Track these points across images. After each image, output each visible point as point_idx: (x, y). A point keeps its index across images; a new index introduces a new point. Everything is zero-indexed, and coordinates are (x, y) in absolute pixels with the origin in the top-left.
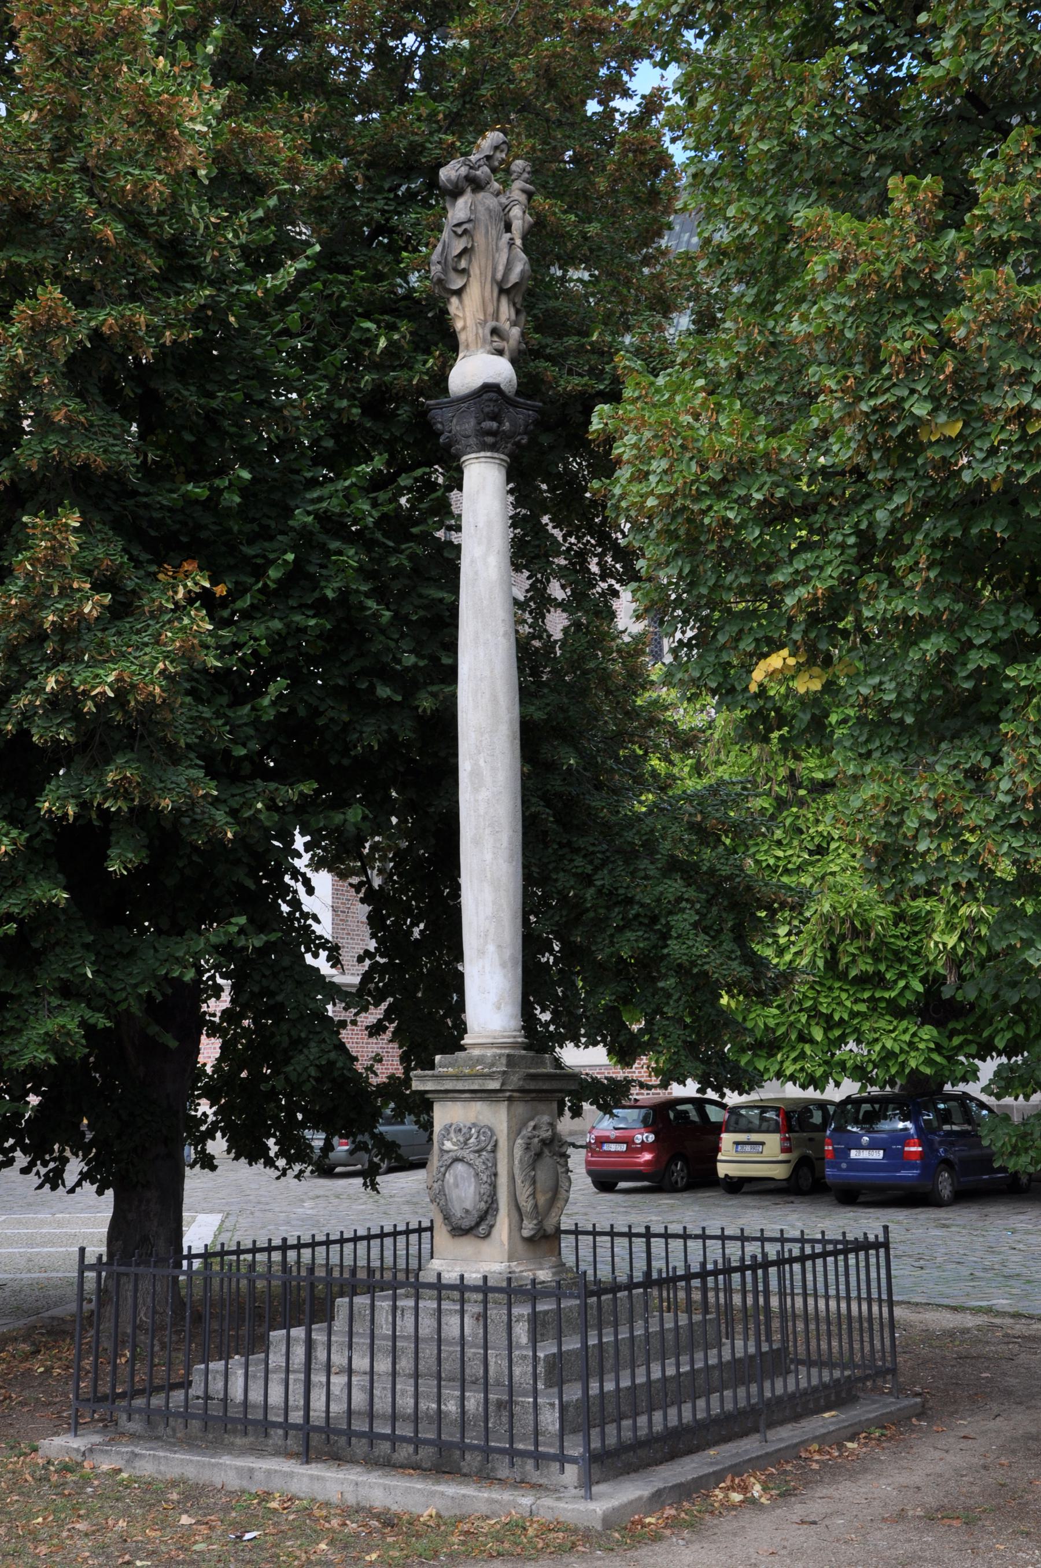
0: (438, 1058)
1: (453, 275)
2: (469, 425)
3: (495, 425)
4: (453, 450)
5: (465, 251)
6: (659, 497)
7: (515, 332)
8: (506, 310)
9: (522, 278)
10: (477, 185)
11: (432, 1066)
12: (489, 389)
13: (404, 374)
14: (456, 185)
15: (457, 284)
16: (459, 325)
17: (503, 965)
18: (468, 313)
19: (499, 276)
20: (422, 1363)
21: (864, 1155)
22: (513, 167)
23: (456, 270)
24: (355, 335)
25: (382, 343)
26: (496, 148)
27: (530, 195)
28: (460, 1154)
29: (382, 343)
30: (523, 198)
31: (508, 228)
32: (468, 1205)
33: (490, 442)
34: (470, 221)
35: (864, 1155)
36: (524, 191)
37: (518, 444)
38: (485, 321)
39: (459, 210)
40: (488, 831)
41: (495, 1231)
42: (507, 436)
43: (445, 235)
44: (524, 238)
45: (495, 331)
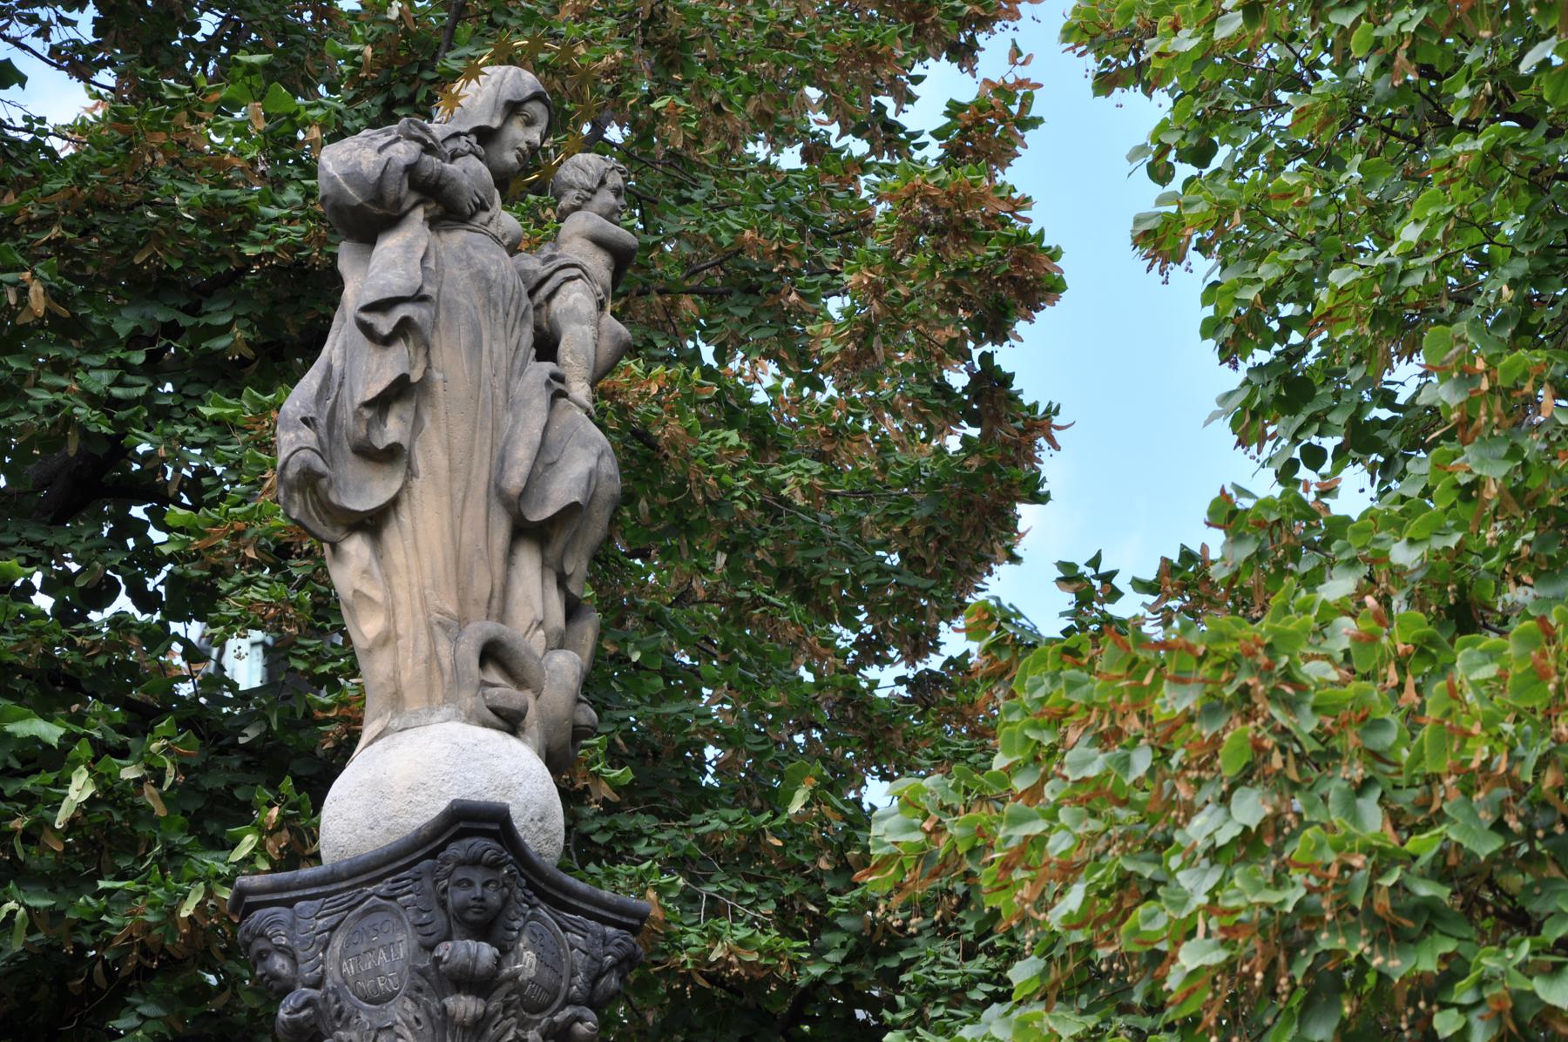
3: (486, 952)
5: (400, 391)
7: (564, 669)
8: (533, 598)
10: (448, 209)
12: (475, 824)
14: (377, 190)
16: (366, 628)
18: (398, 592)
19: (515, 480)
22: (567, 173)
25: (80, 788)
26: (513, 108)
29: (80, 788)
30: (599, 264)
31: (546, 346)
34: (419, 298)
36: (600, 242)
45: (492, 653)
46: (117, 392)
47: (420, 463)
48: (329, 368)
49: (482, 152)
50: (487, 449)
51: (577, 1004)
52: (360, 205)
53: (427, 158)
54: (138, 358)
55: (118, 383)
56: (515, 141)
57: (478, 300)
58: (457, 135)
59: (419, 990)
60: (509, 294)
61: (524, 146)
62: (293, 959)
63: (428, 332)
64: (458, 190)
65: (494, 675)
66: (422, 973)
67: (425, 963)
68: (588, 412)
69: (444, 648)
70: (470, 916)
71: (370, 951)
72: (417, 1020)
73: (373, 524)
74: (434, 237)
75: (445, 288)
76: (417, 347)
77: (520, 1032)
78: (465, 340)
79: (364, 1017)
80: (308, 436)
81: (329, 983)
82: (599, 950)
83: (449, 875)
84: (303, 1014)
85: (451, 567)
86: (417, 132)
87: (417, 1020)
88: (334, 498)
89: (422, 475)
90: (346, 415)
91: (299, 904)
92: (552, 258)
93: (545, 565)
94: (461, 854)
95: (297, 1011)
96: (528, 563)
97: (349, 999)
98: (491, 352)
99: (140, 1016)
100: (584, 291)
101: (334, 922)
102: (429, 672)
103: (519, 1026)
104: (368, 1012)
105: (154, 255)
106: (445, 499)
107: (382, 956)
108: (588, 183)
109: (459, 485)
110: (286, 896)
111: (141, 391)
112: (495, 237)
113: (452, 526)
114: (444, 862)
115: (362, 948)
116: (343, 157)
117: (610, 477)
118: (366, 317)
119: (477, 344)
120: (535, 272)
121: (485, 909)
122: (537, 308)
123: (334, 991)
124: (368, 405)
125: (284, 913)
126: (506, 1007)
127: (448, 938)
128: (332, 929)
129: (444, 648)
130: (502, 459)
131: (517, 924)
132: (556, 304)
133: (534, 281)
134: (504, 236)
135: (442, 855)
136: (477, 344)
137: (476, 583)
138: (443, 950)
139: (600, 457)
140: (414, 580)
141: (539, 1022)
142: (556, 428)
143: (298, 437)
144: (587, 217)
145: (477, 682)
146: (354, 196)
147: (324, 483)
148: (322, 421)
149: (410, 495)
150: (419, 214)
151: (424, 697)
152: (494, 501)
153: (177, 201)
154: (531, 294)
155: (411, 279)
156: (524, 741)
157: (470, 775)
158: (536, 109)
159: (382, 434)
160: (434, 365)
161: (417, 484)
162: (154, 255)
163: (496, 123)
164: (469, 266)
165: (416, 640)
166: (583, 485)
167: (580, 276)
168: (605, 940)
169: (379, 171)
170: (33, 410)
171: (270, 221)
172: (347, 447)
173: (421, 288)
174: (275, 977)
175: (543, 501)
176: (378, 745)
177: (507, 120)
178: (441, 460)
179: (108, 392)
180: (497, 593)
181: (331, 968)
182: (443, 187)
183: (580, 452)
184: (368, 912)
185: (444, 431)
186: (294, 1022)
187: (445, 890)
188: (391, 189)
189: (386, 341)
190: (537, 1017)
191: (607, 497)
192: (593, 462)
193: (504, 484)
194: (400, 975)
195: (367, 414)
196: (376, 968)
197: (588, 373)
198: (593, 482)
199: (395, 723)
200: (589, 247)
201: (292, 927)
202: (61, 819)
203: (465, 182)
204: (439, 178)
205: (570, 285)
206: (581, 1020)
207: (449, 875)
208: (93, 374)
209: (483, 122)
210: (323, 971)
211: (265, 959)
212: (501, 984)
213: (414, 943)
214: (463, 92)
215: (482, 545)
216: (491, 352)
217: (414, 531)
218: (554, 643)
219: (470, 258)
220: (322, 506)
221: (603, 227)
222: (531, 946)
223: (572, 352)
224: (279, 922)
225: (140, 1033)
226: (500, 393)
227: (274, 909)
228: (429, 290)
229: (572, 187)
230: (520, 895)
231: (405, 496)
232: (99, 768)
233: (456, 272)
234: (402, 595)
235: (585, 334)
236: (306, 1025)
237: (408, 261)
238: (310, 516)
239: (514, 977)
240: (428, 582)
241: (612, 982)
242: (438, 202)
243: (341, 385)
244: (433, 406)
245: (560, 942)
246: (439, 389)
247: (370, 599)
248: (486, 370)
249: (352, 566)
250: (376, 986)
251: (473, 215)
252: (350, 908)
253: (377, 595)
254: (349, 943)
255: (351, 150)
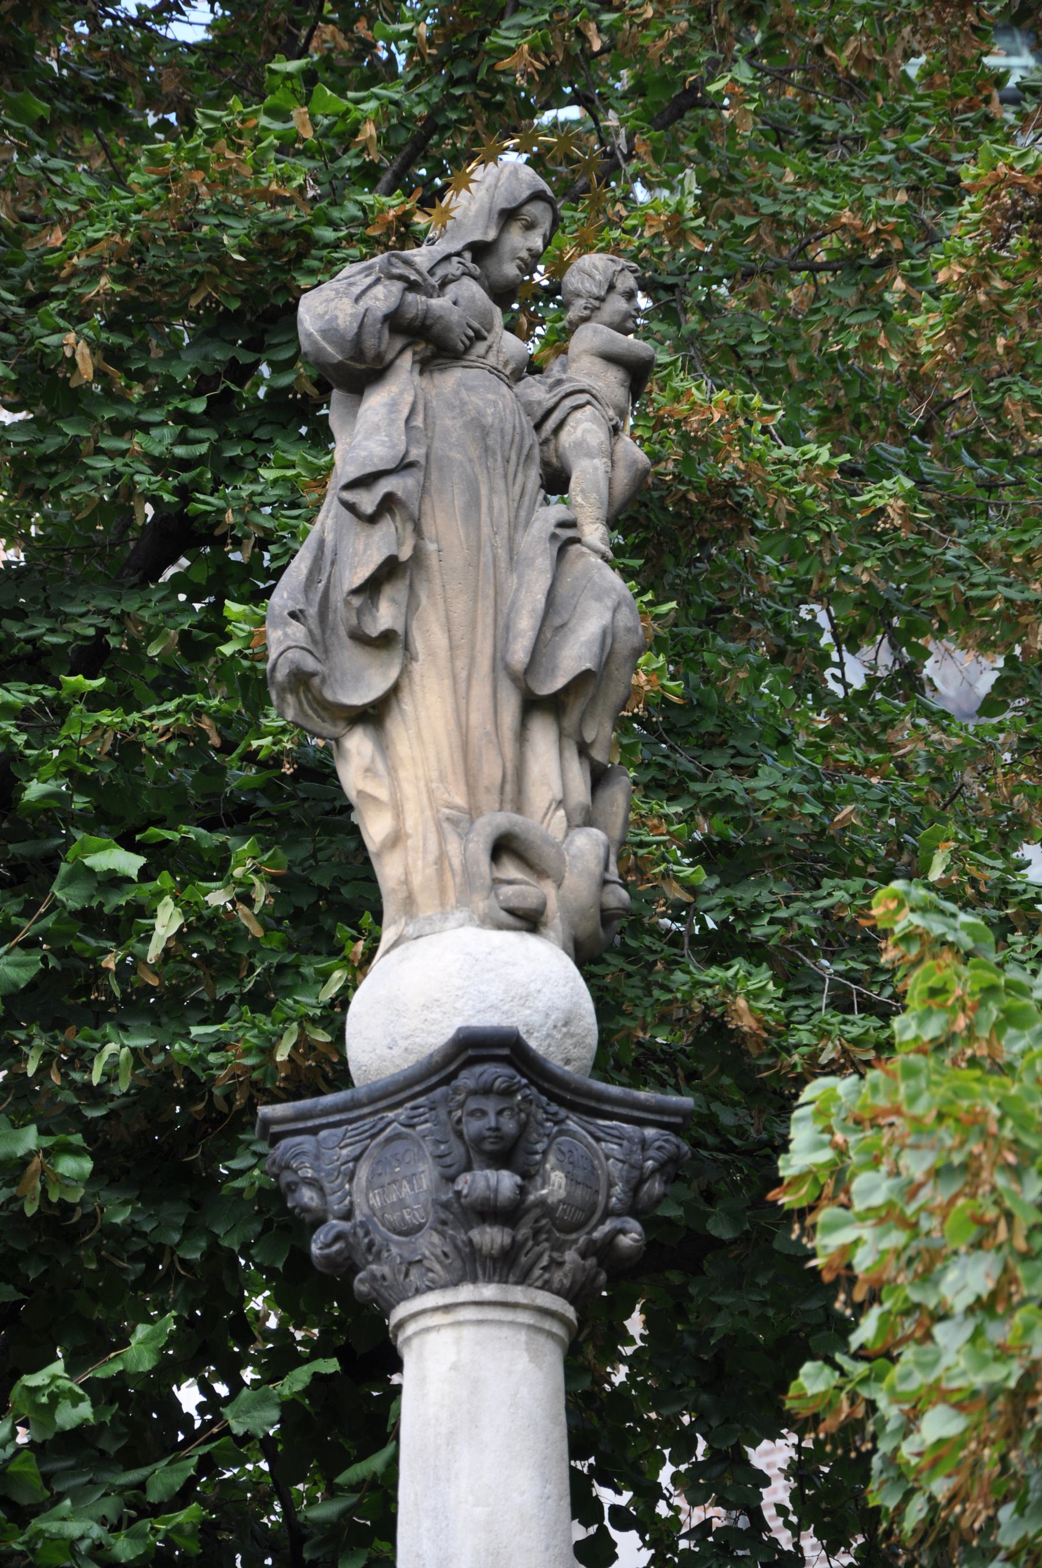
1: (349, 656)
3: (506, 1181)
4: (360, 1285)
5: (390, 570)
6: (965, 1402)
7: (587, 847)
8: (551, 768)
9: (607, 655)
10: (437, 347)
13: (244, 1029)
15: (363, 682)
16: (375, 829)
18: (405, 794)
19: (519, 654)
22: (572, 280)
23: (360, 638)
24: (68, 895)
25: (167, 921)
26: (508, 216)
27: (637, 374)
29: (167, 921)
30: (610, 383)
31: (556, 481)
33: (497, 1244)
34: (404, 466)
36: (611, 358)
37: (604, 1251)
38: (473, 812)
39: (367, 432)
42: (559, 1224)
43: (329, 519)
44: (617, 520)
45: (504, 847)
46: (180, 451)
47: (419, 644)
48: (321, 543)
49: (476, 270)
50: (489, 620)
51: (618, 1215)
52: (340, 363)
53: (410, 297)
54: (198, 406)
55: (182, 439)
56: (514, 250)
57: (474, 451)
58: (447, 258)
59: (444, 1223)
60: (508, 438)
61: (524, 254)
62: (321, 1190)
63: (414, 507)
64: (447, 328)
65: (510, 870)
66: (446, 1206)
67: (447, 1196)
68: (604, 557)
69: (454, 847)
70: (488, 1146)
71: (394, 1182)
72: (445, 1255)
73: (373, 716)
74: (424, 382)
75: (437, 444)
76: (404, 522)
77: (555, 1255)
78: (459, 502)
79: (394, 1250)
80: (297, 631)
81: (358, 1217)
82: (638, 1157)
83: (461, 1105)
84: (336, 1247)
85: (458, 756)
86: (399, 270)
87: (445, 1255)
88: (329, 695)
89: (421, 657)
90: (338, 597)
91: (323, 1133)
92: (559, 382)
93: (561, 735)
94: (471, 1084)
95: (329, 1245)
96: (543, 738)
97: (379, 1231)
98: (491, 508)
99: (255, 1154)
100: (594, 419)
101: (358, 1152)
102: (440, 874)
103: (553, 1249)
104: (398, 1244)
105: (209, 297)
106: (447, 682)
107: (406, 1188)
108: (595, 291)
109: (461, 663)
110: (310, 1123)
111: (203, 449)
112: (494, 371)
113: (457, 711)
114: (456, 1091)
115: (386, 1179)
116: (321, 310)
117: (628, 630)
118: (347, 496)
119: (473, 503)
120: (539, 403)
121: (502, 1138)
122: (545, 442)
123: (362, 1224)
124: (356, 592)
125: (306, 1142)
126: (536, 1233)
127: (468, 1168)
128: (357, 1159)
129: (454, 847)
130: (507, 628)
131: (540, 1147)
132: (566, 437)
133: (539, 413)
134: (506, 364)
135: (454, 1083)
136: (473, 503)
137: (486, 769)
138: (463, 1183)
139: (615, 611)
140: (420, 773)
141: (576, 1241)
142: (567, 580)
143: (286, 634)
144: (595, 331)
145: (488, 882)
146: (334, 354)
147: (316, 681)
148: (312, 611)
149: (411, 680)
150: (406, 361)
151: (437, 902)
152: (502, 675)
153: (226, 240)
154: (538, 427)
155: (393, 447)
156: (546, 937)
157: (484, 988)
158: (538, 210)
159: (375, 619)
160: (426, 534)
161: (416, 667)
162: (209, 297)
163: (491, 235)
164: (462, 413)
165: (425, 839)
166: (596, 649)
167: (588, 403)
168: (644, 1144)
169: (356, 325)
170: (93, 481)
171: (326, 246)
172: (343, 632)
173: (407, 453)
174: (306, 1209)
175: (553, 671)
176: (394, 953)
177: (503, 228)
178: (440, 640)
179: (170, 452)
180: (509, 778)
181: (358, 1199)
182: (431, 326)
183: (595, 606)
184: (389, 1140)
185: (441, 606)
186: (327, 1257)
187: (459, 1121)
188: (370, 343)
189: (372, 519)
190: (574, 1236)
191: (626, 652)
192: (608, 616)
193: (509, 658)
194: (425, 1207)
195: (356, 601)
196: (401, 1200)
197: (602, 513)
198: (609, 641)
199: (410, 930)
200: (599, 364)
201: (317, 1157)
202: (154, 951)
203: (455, 316)
204: (425, 318)
205: (578, 415)
206: (623, 1232)
207: (461, 1105)
208: (154, 432)
209: (477, 236)
210: (351, 1203)
211: (294, 1191)
212: (528, 1210)
213: (436, 1174)
214: (452, 205)
215: (489, 727)
216: (491, 508)
217: (417, 719)
218: (578, 819)
219: (463, 403)
220: (318, 702)
221: (612, 340)
222: (560, 1166)
223: (582, 491)
224: (303, 1153)
225: (256, 1172)
226: (502, 553)
227: (298, 1139)
228: (416, 453)
229: (578, 295)
230: (541, 1115)
231: (405, 682)
232: (185, 896)
233: (448, 422)
234: (408, 789)
235: (596, 469)
236: (340, 1259)
237: (392, 422)
238: (307, 716)
239: (542, 1202)
240: (434, 775)
241: (655, 1187)
242: (428, 341)
243: (333, 563)
244: (429, 581)
245: (595, 1153)
246: (433, 561)
247: (374, 799)
248: (486, 530)
249: (357, 761)
250: (403, 1219)
251: (467, 349)
252: (373, 1137)
253: (382, 793)
254: (373, 1174)
255: (328, 301)
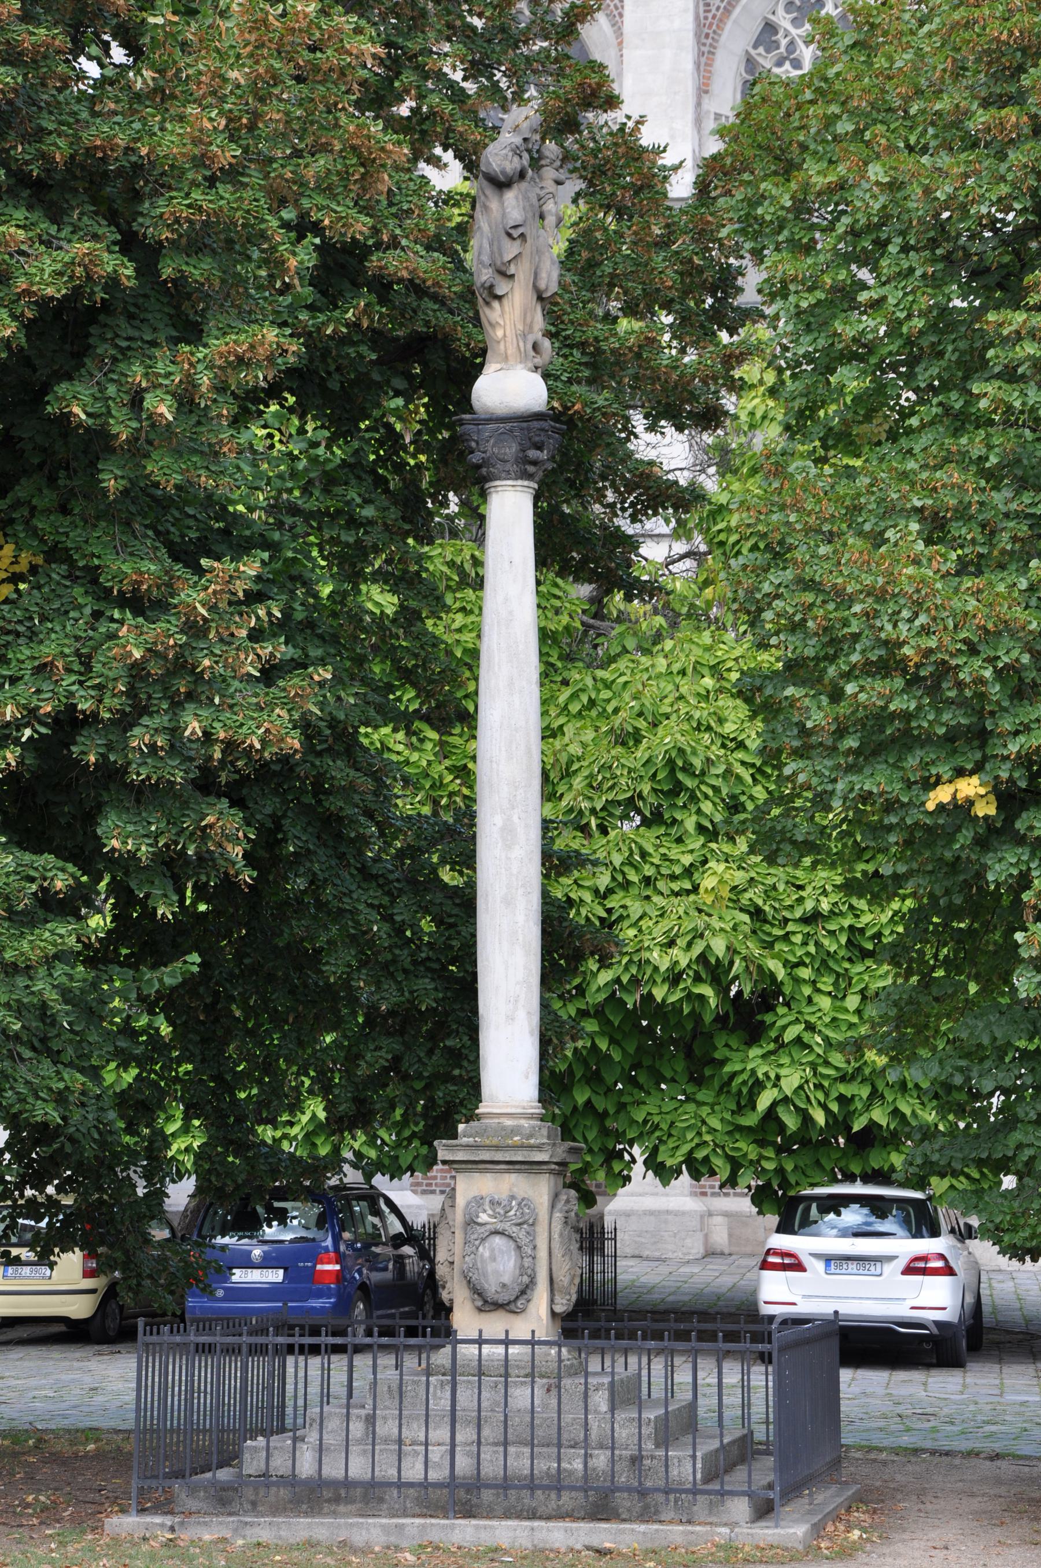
0: (461, 1127)
2: (510, 450)
11: (455, 1136)
17: (531, 1033)
20: (510, 1431)
21: (255, 1276)
28: (500, 1227)
32: (506, 1279)
35: (255, 1276)
40: (520, 891)
41: (532, 1306)
